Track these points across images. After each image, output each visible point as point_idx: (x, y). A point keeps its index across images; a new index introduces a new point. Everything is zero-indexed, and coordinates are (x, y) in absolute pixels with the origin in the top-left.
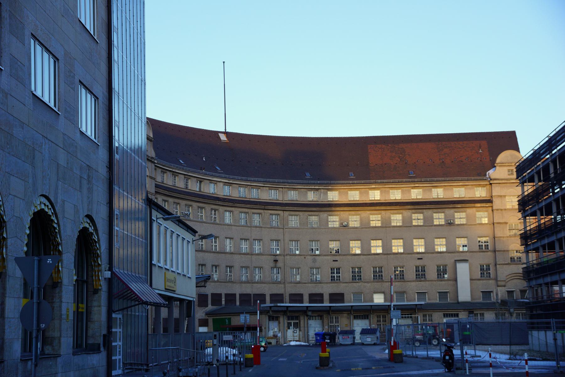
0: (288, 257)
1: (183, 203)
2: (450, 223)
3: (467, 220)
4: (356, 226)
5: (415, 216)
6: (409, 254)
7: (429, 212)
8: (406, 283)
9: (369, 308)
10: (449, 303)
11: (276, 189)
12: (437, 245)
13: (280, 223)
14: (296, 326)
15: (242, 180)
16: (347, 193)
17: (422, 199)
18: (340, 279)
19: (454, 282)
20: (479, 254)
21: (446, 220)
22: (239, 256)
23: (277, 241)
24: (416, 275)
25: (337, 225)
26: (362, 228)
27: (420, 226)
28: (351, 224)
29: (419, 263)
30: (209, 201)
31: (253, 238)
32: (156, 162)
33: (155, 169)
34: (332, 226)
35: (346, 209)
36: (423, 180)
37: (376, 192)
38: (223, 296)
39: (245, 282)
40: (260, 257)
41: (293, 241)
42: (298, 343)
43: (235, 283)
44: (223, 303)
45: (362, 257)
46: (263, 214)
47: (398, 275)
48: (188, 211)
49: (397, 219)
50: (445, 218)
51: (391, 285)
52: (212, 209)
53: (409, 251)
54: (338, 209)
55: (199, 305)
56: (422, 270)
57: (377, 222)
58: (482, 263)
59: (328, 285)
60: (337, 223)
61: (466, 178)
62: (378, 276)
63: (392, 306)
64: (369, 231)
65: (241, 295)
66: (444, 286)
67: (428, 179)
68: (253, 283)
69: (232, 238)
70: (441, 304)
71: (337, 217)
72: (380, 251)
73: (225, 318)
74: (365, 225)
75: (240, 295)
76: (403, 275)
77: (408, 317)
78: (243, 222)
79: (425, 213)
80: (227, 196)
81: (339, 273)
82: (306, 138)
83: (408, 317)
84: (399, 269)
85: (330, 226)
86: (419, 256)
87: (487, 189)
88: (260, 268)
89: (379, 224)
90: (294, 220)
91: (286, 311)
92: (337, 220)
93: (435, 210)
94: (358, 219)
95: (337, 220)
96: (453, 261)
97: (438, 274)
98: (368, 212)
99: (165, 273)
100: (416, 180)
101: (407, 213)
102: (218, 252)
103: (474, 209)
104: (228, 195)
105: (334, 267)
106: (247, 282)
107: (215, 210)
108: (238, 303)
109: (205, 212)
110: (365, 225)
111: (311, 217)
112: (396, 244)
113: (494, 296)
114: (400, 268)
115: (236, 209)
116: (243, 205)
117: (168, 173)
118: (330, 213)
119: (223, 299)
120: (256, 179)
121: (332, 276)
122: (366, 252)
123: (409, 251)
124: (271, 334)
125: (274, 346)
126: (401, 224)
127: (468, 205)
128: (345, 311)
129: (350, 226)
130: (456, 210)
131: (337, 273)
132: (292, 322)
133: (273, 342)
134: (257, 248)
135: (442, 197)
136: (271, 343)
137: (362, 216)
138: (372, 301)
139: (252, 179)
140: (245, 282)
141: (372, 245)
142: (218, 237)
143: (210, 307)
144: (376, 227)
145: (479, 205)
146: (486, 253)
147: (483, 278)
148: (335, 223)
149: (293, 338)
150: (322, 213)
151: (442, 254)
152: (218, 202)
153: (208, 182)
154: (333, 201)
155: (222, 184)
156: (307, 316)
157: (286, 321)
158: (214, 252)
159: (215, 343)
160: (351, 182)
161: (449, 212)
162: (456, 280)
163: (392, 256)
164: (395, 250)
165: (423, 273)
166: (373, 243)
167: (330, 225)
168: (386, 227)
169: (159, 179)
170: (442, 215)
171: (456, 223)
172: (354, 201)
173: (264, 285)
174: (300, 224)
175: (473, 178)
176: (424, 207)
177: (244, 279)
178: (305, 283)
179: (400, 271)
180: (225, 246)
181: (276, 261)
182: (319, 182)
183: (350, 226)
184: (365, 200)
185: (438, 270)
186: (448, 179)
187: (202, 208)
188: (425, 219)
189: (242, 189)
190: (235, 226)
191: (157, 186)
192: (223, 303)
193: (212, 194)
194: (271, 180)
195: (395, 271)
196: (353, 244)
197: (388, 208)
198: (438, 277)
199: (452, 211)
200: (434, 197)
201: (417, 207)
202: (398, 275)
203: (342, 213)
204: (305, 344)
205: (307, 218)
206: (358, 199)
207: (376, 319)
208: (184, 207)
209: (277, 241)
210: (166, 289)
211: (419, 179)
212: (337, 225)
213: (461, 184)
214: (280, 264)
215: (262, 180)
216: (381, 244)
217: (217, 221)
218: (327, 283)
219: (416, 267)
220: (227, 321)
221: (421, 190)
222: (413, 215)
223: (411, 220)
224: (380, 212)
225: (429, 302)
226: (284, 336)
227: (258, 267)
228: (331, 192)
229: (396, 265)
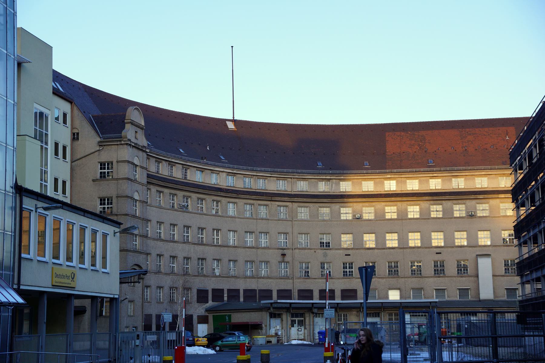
0: (297, 251)
1: (181, 194)
2: (471, 216)
3: (490, 212)
4: (370, 218)
5: (434, 208)
6: (426, 248)
7: (449, 203)
8: (424, 279)
9: (380, 305)
10: (470, 301)
11: (284, 179)
12: (457, 239)
13: (289, 215)
14: (301, 323)
15: (247, 170)
16: (361, 184)
17: (441, 189)
18: (352, 275)
19: (476, 279)
20: (502, 248)
21: (467, 212)
22: (243, 250)
23: (286, 233)
24: (435, 270)
25: (350, 217)
26: (376, 220)
27: (439, 218)
28: (366, 217)
29: (438, 258)
30: (210, 192)
31: (259, 231)
32: (148, 151)
33: (148, 158)
34: (345, 218)
35: (359, 200)
36: (442, 169)
37: (392, 182)
38: (242, 293)
39: (250, 277)
40: (266, 251)
41: (302, 234)
42: (300, 342)
43: (239, 278)
44: (226, 299)
45: (376, 251)
46: (270, 206)
47: (414, 271)
48: (187, 202)
49: (414, 211)
50: (466, 210)
51: (327, 281)
52: (213, 201)
53: (426, 245)
54: (351, 200)
55: (198, 301)
56: (440, 265)
57: (393, 214)
58: (507, 258)
59: (340, 281)
60: (351, 215)
61: (489, 167)
62: (393, 271)
63: (327, 304)
64: (388, 223)
65: (245, 291)
66: (465, 282)
67: (448, 168)
68: (258, 278)
69: (236, 231)
70: (461, 301)
71: (350, 209)
72: (395, 244)
73: (225, 315)
74: (380, 218)
75: (245, 291)
76: (420, 271)
77: (422, 315)
78: (248, 214)
79: (445, 205)
80: (230, 187)
81: (352, 268)
82: (320, 125)
83: (422, 315)
84: (416, 264)
85: (342, 218)
86: (438, 250)
87: (512, 178)
88: (267, 262)
89: (395, 216)
90: (303, 212)
91: (290, 309)
92: (350, 212)
93: (455, 202)
94: (373, 211)
95: (350, 212)
96: (474, 255)
97: (458, 270)
98: (383, 204)
99: (52, 268)
100: (435, 169)
101: (425, 204)
102: (220, 246)
103: (498, 200)
104: (232, 185)
105: (346, 261)
106: (252, 277)
107: (218, 202)
108: (242, 299)
109: (206, 204)
110: (380, 218)
111: (322, 209)
112: (413, 238)
113: (519, 293)
114: (418, 263)
115: (241, 200)
116: (248, 197)
117: (164, 162)
118: (343, 204)
119: (226, 295)
120: (263, 169)
121: (344, 271)
122: (381, 246)
123: (426, 245)
124: (272, 332)
125: (274, 345)
126: (418, 216)
127: (490, 196)
128: (354, 308)
129: (364, 218)
130: (478, 201)
131: (349, 268)
132: (297, 319)
133: (274, 340)
134: (264, 241)
135: (463, 187)
136: (271, 342)
137: (377, 207)
138: (387, 297)
139: (259, 169)
140: (250, 277)
141: (387, 238)
142: (220, 230)
143: (210, 303)
144: (391, 219)
145: (502, 196)
146: (510, 248)
147: (507, 274)
148: (348, 215)
149: (296, 336)
150: (333, 205)
151: (463, 248)
152: (219, 193)
153: (210, 171)
154: (345, 192)
155: (225, 174)
156: (313, 313)
157: (289, 319)
158: (215, 246)
159: (137, 344)
160: (365, 172)
161: (471, 203)
162: (477, 276)
163: (408, 250)
164: (458, 243)
165: (442, 268)
166: (388, 236)
167: (343, 217)
168: (402, 219)
169: (153, 168)
170: (463, 207)
171: (478, 215)
172: (368, 191)
173: (270, 280)
174: (310, 216)
175: (497, 167)
176: (443, 198)
177: (248, 273)
178: (315, 279)
179: (417, 266)
180: (228, 239)
181: (284, 255)
182: (331, 172)
183: (364, 218)
184: (380, 190)
185: (458, 265)
186: (469, 168)
187: (202, 200)
188: (444, 211)
189: (247, 180)
190: (239, 218)
191: (149, 176)
192: (226, 299)
193: (214, 184)
194: (279, 170)
195: (412, 266)
196: (366, 237)
197: (405, 199)
198: (458, 273)
199: (474, 202)
200: (454, 187)
201: (435, 198)
202: (414, 271)
203: (355, 204)
204: (307, 343)
205: (318, 210)
206: (372, 190)
207: (387, 317)
208: (181, 198)
209: (286, 233)
210: (53, 285)
211: (438, 169)
212: (350, 217)
213: (483, 173)
214: (287, 259)
215: (269, 169)
216: (396, 238)
217: (220, 213)
218: (339, 278)
219: (434, 262)
220: (227, 318)
221: (440, 180)
222: (432, 206)
223: (429, 212)
224: (396, 203)
225: (449, 299)
226: (287, 335)
227: (264, 262)
228: (344, 183)
229: (413, 259)
